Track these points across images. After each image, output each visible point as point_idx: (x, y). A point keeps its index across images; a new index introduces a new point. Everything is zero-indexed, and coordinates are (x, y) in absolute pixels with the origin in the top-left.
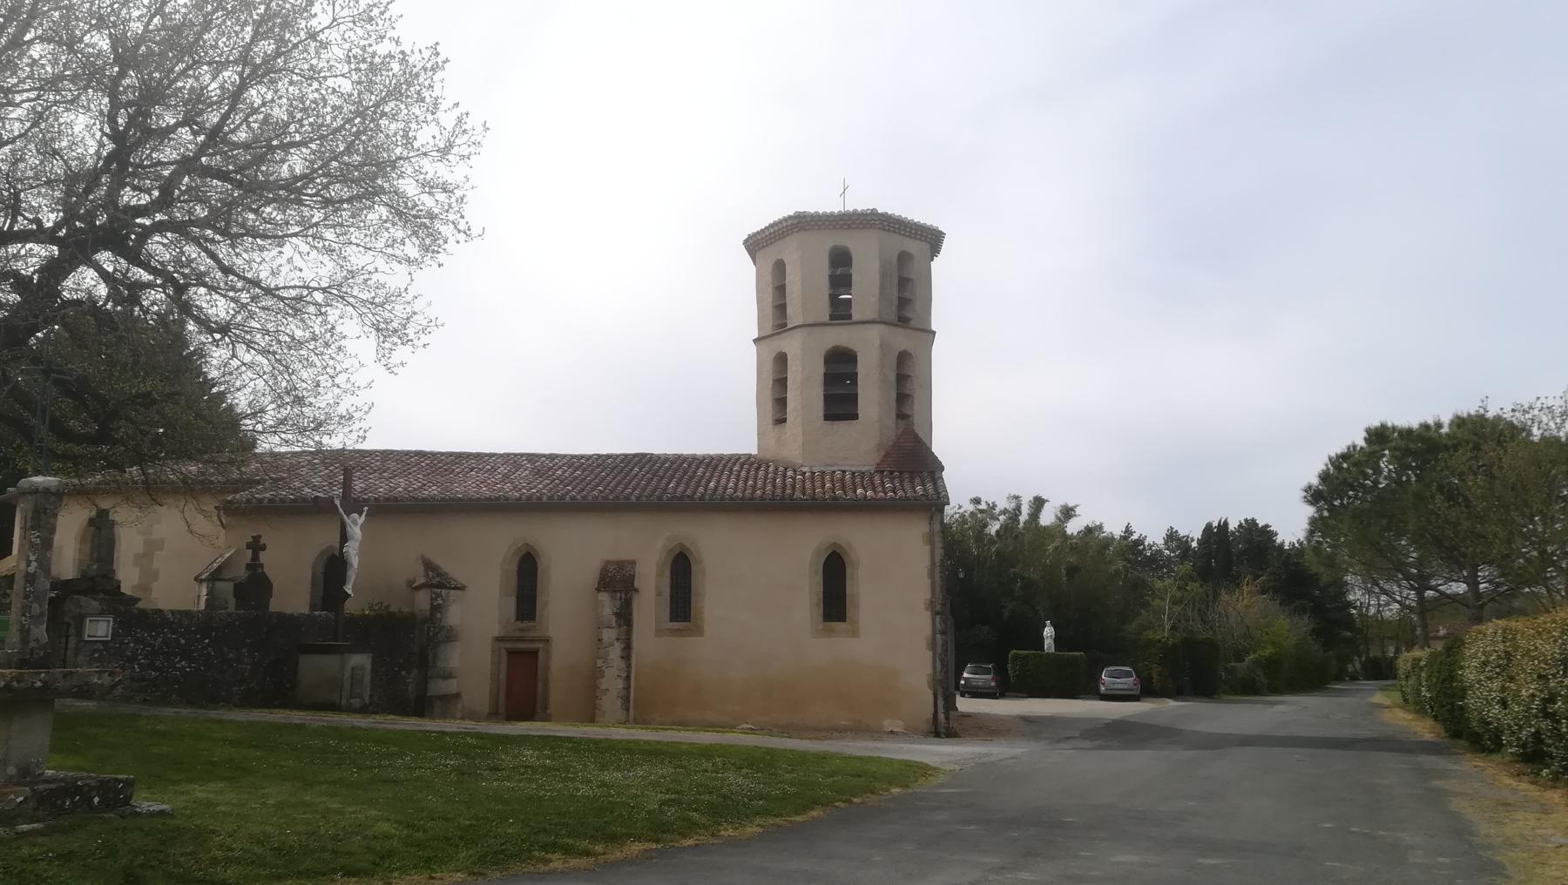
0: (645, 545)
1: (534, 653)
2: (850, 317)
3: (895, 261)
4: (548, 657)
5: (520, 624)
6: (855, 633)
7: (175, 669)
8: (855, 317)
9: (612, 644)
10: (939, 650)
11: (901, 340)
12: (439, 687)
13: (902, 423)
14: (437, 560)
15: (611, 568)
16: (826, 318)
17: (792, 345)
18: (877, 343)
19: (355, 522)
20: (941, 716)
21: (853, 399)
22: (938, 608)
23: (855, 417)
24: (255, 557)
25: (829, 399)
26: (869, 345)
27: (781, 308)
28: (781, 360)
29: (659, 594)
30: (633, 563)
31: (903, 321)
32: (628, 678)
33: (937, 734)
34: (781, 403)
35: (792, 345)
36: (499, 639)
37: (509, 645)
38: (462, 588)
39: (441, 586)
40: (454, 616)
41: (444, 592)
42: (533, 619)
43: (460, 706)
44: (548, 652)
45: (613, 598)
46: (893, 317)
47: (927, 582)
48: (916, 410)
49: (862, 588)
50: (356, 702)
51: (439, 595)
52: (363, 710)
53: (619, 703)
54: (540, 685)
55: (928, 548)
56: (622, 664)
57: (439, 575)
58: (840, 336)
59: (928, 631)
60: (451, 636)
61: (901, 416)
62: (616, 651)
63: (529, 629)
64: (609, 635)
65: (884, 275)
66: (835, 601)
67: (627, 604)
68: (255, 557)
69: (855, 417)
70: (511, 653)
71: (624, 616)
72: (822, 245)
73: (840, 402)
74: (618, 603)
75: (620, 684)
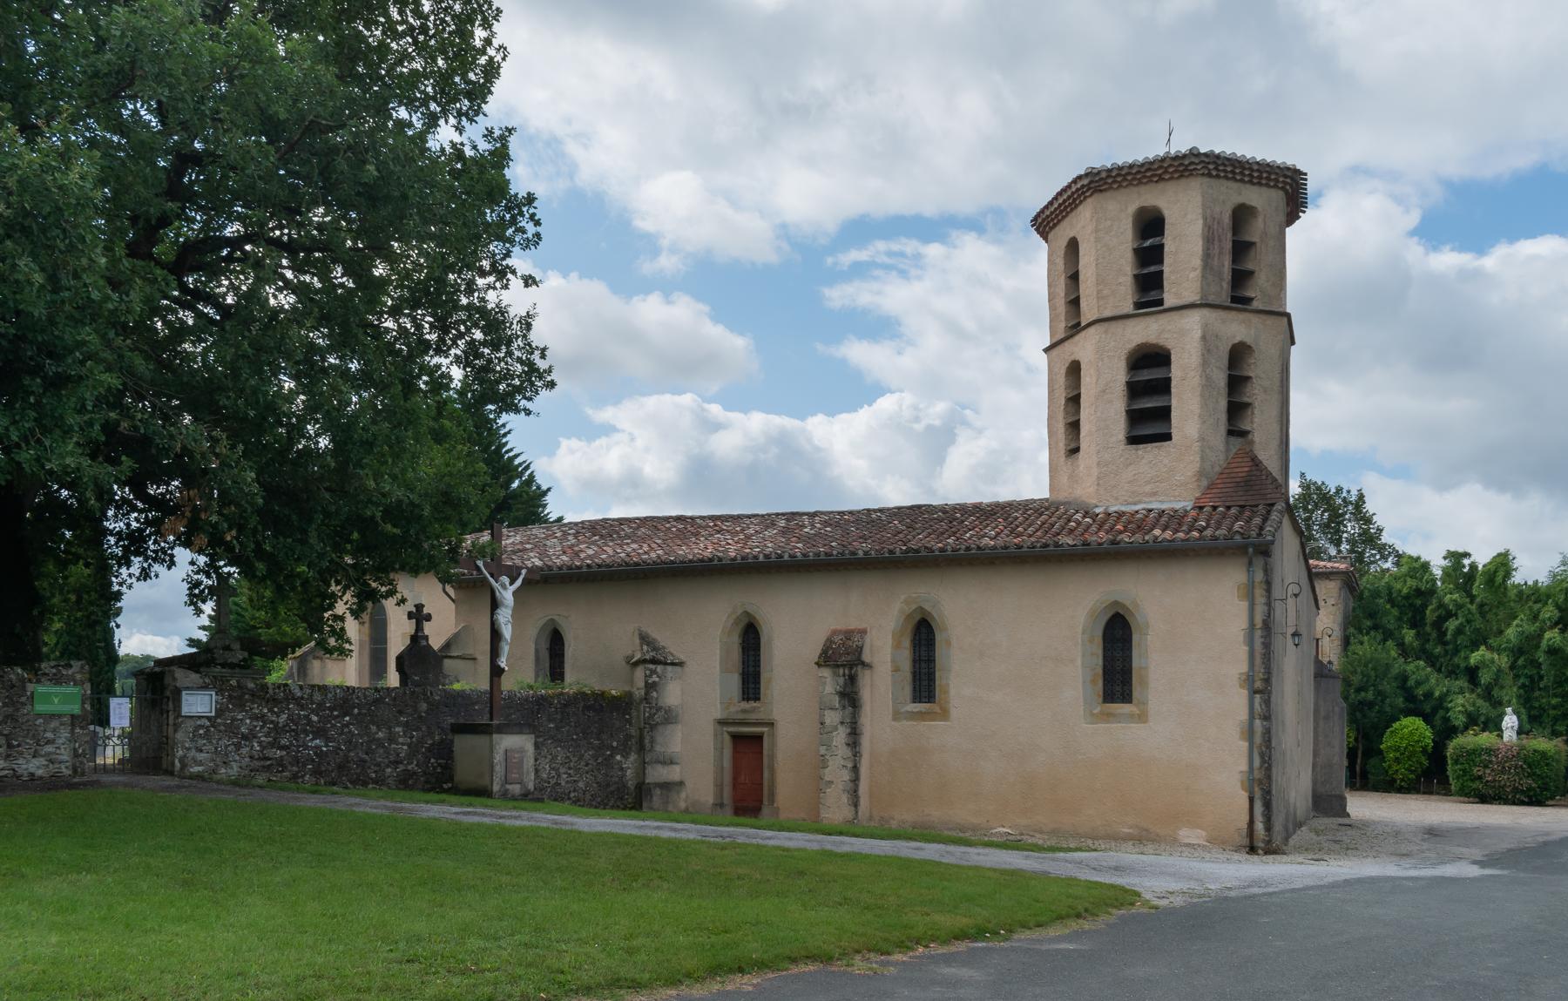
0: (877, 615)
1: (758, 738)
2: (1160, 302)
3: (1227, 219)
4: (773, 745)
5: (745, 705)
6: (1142, 718)
7: (307, 748)
8: (1168, 303)
9: (836, 729)
10: (1258, 739)
11: (1236, 328)
12: (656, 774)
13: (1237, 442)
14: (654, 634)
15: (837, 639)
16: (1127, 307)
17: (1084, 348)
18: (1198, 334)
19: (504, 587)
20: (1259, 826)
21: (1164, 414)
22: (1258, 685)
23: (1167, 437)
24: (419, 627)
25: (1135, 417)
26: (1187, 338)
27: (1074, 303)
29: (896, 670)
30: (863, 632)
31: (1239, 301)
32: (855, 769)
33: (1252, 850)
34: (1074, 427)
36: (721, 723)
37: (732, 729)
38: (681, 664)
39: (654, 661)
40: (673, 694)
41: (659, 668)
42: (757, 699)
43: (683, 795)
44: (773, 735)
45: (836, 675)
46: (1225, 298)
47: (1243, 651)
49: (1153, 658)
50: (516, 789)
51: (653, 672)
52: (530, 798)
53: (845, 798)
54: (766, 774)
55: (1245, 605)
56: (848, 752)
57: (655, 649)
59: (1244, 715)
60: (670, 717)
61: (1235, 432)
62: (840, 736)
63: (754, 710)
64: (832, 718)
65: (1209, 239)
66: (1117, 677)
67: (852, 679)
68: (419, 627)
69: (1167, 437)
70: (736, 738)
71: (850, 697)
73: (1148, 419)
74: (841, 681)
75: (846, 776)
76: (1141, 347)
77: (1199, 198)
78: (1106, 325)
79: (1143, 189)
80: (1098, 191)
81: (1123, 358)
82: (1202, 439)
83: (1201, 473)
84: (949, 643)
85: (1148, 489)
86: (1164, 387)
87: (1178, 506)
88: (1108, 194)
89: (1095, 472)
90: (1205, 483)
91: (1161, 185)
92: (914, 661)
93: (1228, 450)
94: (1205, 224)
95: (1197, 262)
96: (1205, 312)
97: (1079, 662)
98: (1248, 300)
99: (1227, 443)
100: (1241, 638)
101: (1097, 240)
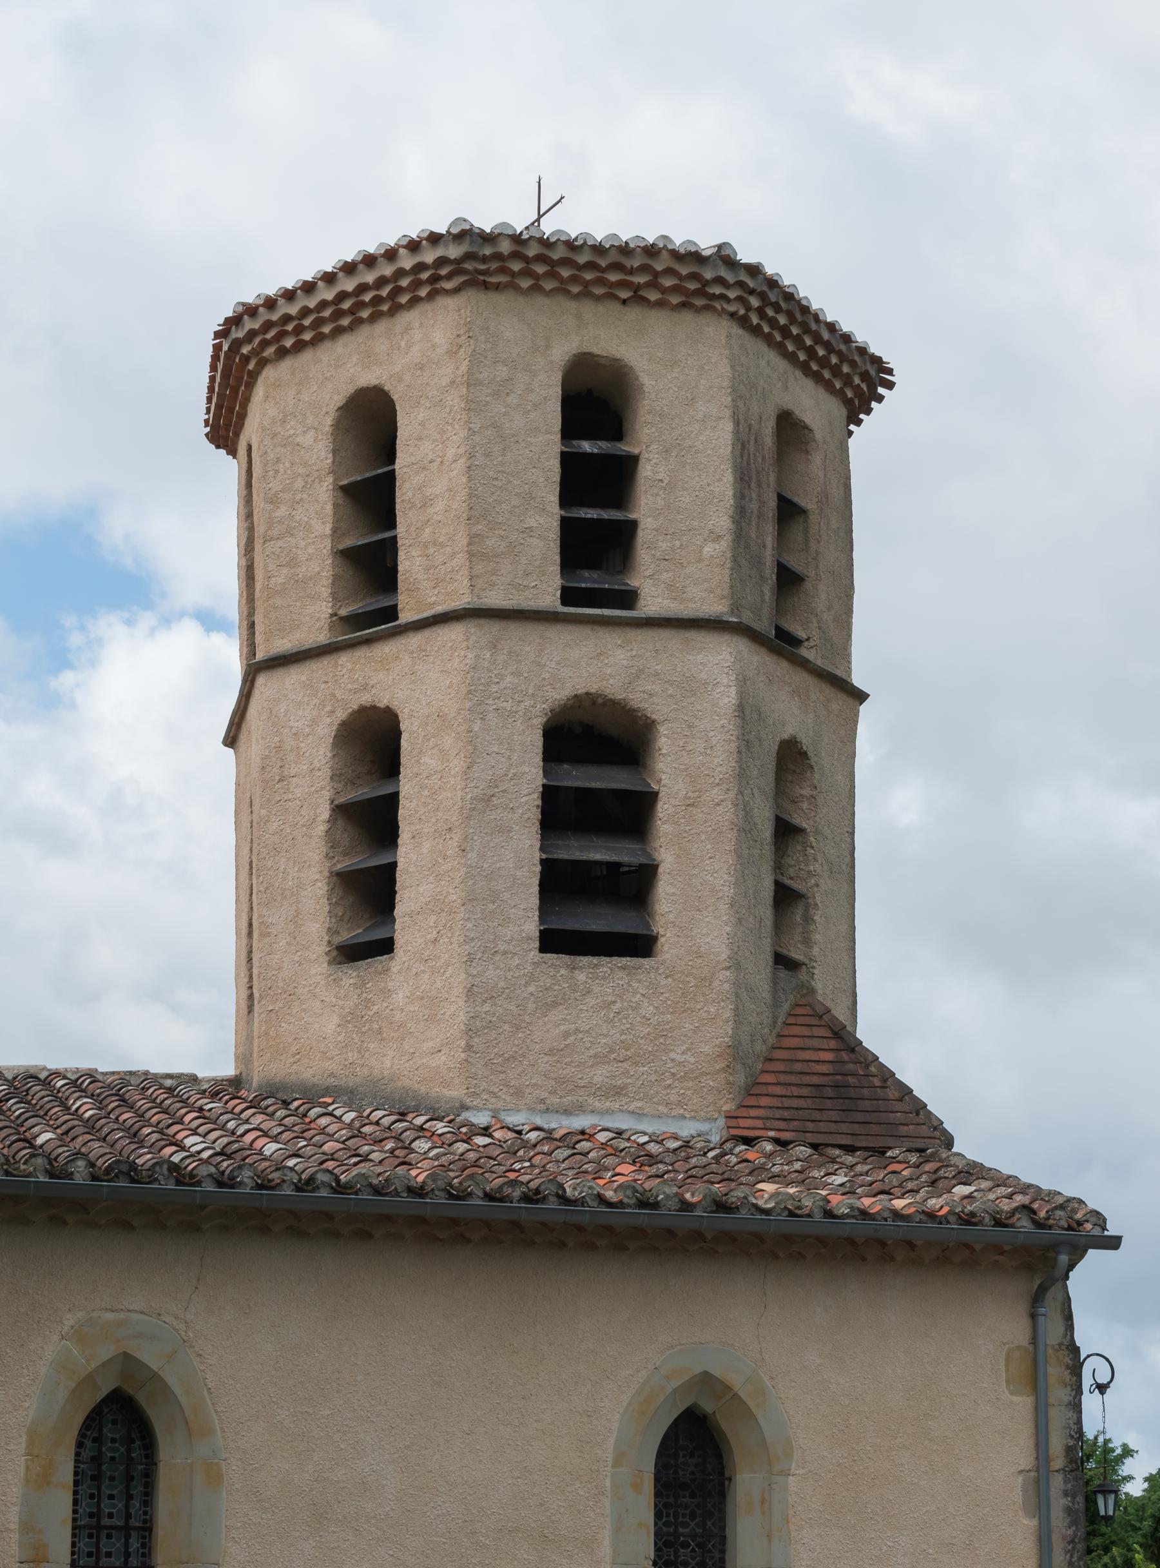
2: (628, 599)
8: (653, 602)
16: (546, 591)
17: (419, 680)
18: (728, 698)
21: (634, 885)
23: (640, 945)
25: (558, 883)
26: (697, 709)
28: (374, 742)
35: (419, 680)
46: (764, 625)
48: (819, 948)
55: (1023, 1404)
58: (591, 663)
69: (640, 945)
72: (541, 344)
73: (594, 898)
76: (363, 710)
77: (724, 369)
78: (494, 628)
79: (588, 309)
80: (478, 283)
81: (539, 722)
82: (735, 964)
83: (735, 1052)
84: (214, 1476)
85: (600, 1075)
86: (633, 813)
87: (687, 1129)
88: (500, 299)
89: (456, 1011)
90: (740, 1079)
91: (633, 313)
92: (147, 1529)
93: (776, 1004)
94: (736, 432)
95: (722, 521)
96: (742, 645)
97: (606, 1549)
98: (796, 642)
99: (775, 982)
100: (1018, 1496)
101: (472, 406)
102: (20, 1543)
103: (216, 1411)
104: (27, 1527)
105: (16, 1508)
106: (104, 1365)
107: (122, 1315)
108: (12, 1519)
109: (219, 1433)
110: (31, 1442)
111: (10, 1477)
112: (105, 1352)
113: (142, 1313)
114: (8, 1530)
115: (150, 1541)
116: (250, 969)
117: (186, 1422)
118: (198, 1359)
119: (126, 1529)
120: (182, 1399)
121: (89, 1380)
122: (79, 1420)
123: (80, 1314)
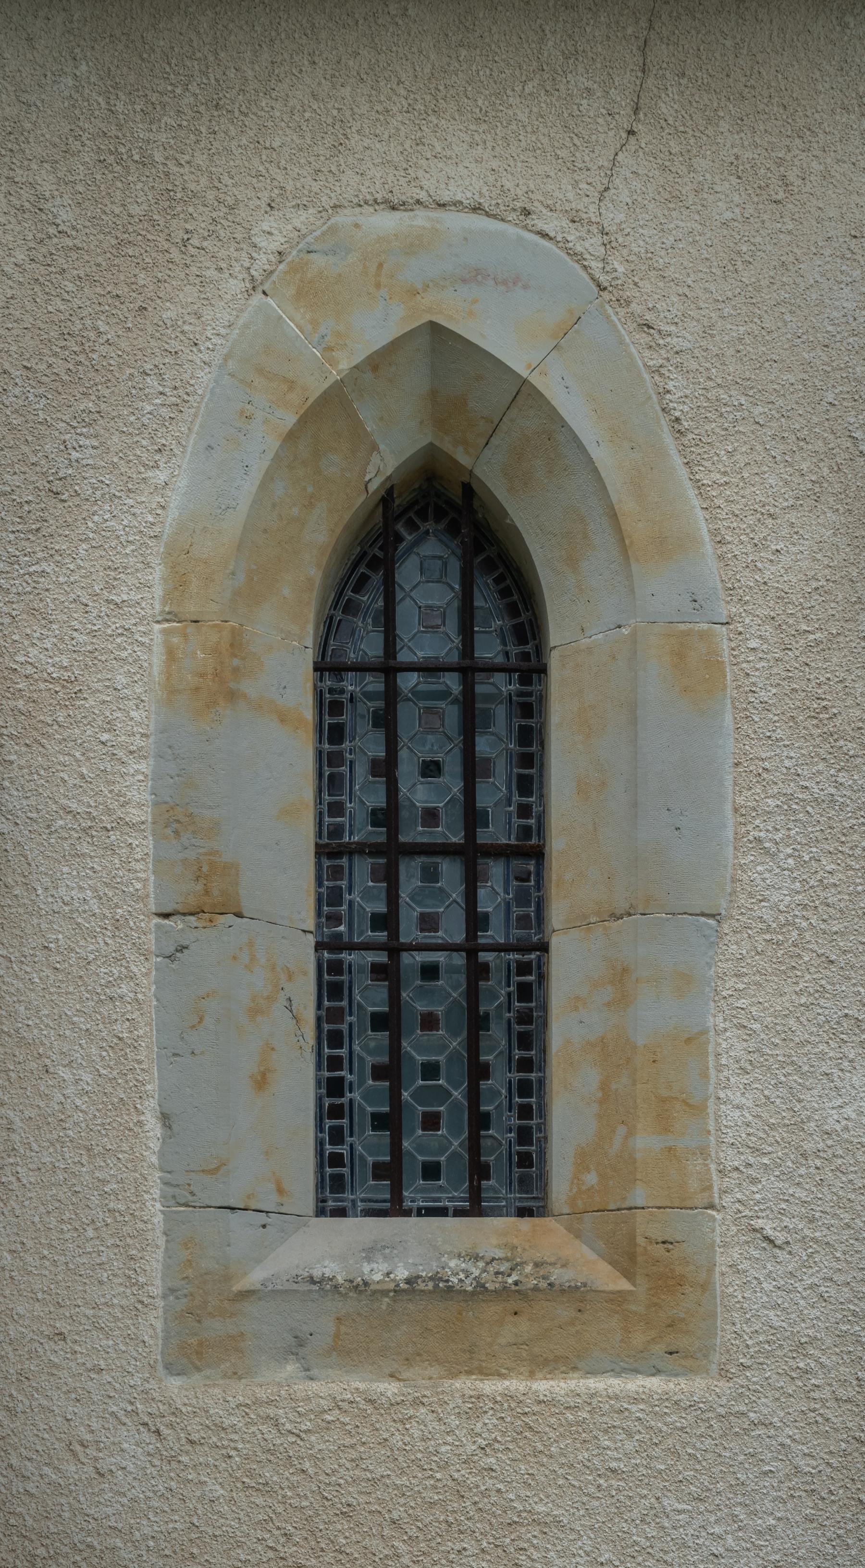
29: (207, 900)
102: (157, 861)
103: (699, 485)
104: (175, 818)
105: (143, 766)
106: (377, 362)
107: (421, 219)
108: (134, 795)
109: (709, 548)
110: (178, 583)
111: (121, 680)
112: (376, 327)
113: (477, 209)
114: (122, 823)
115: (539, 886)
116: (703, 915)
117: (613, 516)
118: (644, 339)
119: (471, 855)
120: (601, 455)
121: (328, 415)
122: (319, 538)
123: (300, 219)
